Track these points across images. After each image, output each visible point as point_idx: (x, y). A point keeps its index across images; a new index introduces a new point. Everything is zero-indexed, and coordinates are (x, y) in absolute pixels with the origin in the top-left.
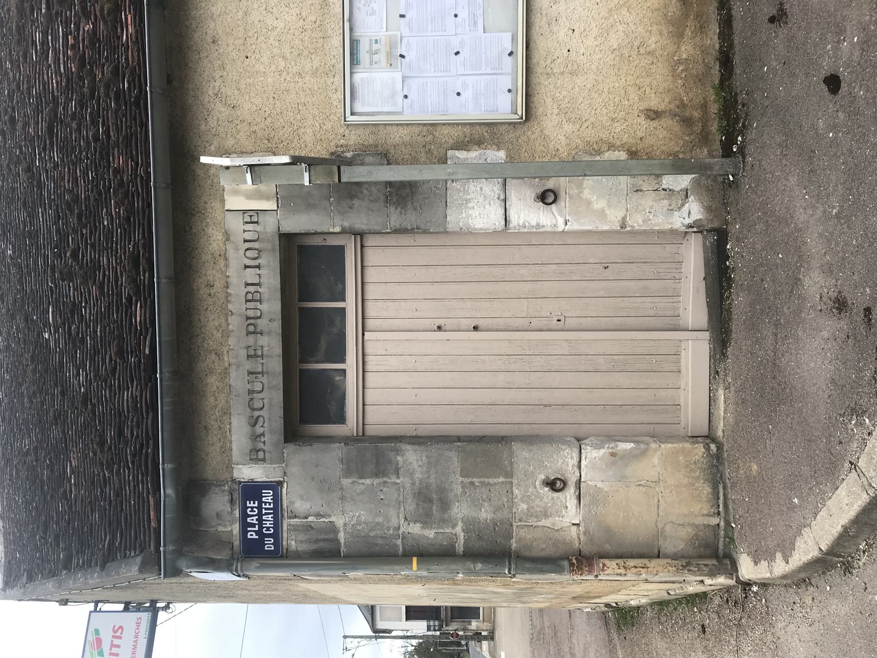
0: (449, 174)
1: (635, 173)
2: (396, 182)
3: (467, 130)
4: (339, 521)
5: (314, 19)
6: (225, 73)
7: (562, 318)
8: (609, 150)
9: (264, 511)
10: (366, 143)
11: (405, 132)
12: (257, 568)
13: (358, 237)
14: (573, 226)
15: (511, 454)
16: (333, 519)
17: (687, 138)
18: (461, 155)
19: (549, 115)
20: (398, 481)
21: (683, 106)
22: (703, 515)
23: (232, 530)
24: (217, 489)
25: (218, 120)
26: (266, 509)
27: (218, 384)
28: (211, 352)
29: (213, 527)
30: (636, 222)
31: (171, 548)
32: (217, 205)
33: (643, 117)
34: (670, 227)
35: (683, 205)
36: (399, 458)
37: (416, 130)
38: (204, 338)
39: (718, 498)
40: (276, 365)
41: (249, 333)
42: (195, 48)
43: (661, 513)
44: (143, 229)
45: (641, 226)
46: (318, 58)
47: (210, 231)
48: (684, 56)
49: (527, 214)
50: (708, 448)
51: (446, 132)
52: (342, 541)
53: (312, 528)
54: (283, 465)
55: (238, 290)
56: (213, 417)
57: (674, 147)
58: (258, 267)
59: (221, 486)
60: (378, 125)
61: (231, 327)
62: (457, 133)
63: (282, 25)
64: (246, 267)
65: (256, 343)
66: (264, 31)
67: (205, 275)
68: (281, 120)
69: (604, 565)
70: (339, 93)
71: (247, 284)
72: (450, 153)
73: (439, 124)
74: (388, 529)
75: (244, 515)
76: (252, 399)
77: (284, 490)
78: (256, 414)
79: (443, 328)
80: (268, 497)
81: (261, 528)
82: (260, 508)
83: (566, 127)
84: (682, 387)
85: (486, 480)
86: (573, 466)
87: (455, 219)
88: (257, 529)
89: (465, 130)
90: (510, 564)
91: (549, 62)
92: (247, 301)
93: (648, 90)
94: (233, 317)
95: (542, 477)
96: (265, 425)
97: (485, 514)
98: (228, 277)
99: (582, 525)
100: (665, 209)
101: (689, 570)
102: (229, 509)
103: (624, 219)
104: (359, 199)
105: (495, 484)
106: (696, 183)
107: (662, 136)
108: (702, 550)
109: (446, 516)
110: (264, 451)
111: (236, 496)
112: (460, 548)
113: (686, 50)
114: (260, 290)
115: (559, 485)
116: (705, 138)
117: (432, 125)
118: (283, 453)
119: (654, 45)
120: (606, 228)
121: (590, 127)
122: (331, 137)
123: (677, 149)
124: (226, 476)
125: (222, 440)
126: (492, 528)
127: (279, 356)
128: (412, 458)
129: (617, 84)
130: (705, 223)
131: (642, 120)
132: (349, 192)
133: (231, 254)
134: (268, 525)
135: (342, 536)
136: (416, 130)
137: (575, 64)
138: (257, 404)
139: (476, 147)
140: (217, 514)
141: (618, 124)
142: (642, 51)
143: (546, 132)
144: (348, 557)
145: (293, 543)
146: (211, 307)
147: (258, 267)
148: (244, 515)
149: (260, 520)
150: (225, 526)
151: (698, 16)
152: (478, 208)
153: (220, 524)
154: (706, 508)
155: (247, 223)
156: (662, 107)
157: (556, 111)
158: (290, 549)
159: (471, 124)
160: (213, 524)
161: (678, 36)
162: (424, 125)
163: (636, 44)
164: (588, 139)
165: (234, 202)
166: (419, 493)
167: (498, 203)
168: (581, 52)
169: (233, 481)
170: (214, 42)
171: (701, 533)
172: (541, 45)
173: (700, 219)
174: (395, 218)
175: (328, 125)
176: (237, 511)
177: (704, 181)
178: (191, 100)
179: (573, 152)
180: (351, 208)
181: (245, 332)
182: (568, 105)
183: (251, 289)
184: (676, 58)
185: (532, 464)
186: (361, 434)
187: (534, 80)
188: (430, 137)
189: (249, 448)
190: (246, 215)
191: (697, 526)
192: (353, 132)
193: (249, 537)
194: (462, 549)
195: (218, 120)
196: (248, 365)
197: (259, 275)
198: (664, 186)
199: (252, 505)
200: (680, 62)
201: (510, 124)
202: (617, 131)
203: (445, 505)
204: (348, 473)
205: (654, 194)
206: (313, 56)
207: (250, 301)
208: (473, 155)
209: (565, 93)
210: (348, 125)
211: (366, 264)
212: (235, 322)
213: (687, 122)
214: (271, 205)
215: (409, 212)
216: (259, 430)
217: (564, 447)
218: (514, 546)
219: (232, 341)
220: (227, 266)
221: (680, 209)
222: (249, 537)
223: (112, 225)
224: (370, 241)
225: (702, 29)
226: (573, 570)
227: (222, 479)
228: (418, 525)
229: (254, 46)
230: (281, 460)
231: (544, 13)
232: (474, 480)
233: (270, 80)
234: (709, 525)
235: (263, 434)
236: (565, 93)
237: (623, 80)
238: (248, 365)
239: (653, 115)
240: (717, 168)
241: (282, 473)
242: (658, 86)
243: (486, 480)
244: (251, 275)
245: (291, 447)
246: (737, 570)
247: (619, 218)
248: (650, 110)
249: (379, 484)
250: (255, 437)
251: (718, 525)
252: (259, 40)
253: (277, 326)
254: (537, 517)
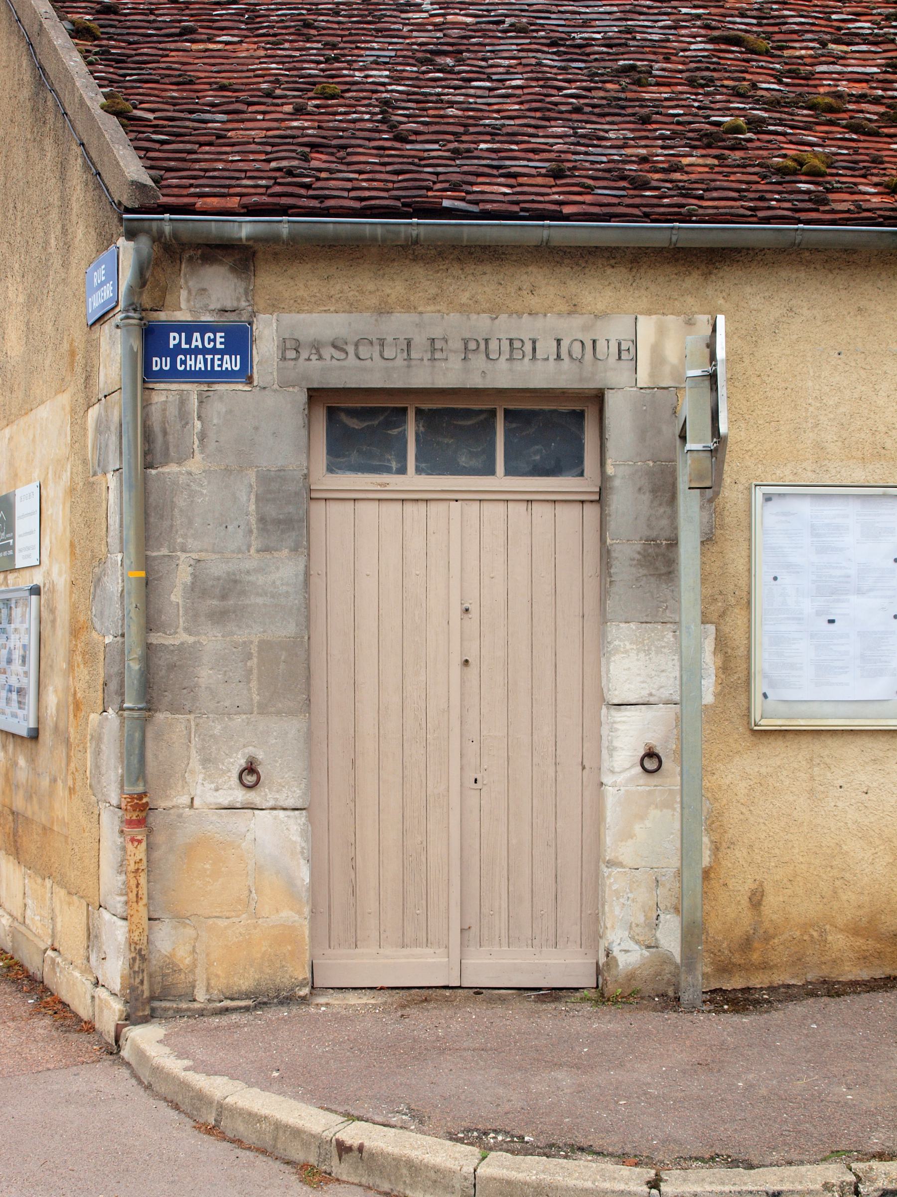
0: (688, 628)
1: (685, 874)
2: (677, 553)
3: (741, 651)
4: (196, 464)
5: (888, 446)
6: (819, 323)
7: (479, 786)
8: (712, 842)
9: (209, 357)
10: (726, 513)
11: (740, 567)
12: (132, 348)
13: (596, 497)
14: (610, 793)
15: (291, 713)
16: (198, 456)
17: (725, 945)
18: (709, 645)
19: (759, 761)
20: (252, 551)
21: (767, 938)
22: (208, 979)
23: (180, 309)
24: (242, 291)
25: (758, 311)
26: (213, 360)
27: (393, 296)
28: (440, 287)
29: (186, 282)
30: (614, 881)
31: (167, 228)
32: (644, 303)
33: (754, 886)
34: (609, 925)
35: (637, 942)
36: (286, 552)
37: (743, 583)
38: (459, 278)
39: (232, 999)
40: (420, 379)
41: (466, 342)
42: (852, 284)
43: (210, 921)
44: (614, 205)
45: (610, 887)
46: (838, 451)
47: (608, 293)
48: (830, 938)
49: (629, 734)
50: (302, 985)
51: (739, 622)
52: (166, 469)
53: (184, 426)
54: (276, 386)
55: (526, 328)
56: (346, 288)
57: (715, 925)
58: (559, 357)
59: (246, 294)
60: (750, 530)
61: (474, 317)
62: (738, 637)
63: (881, 403)
64: (559, 341)
65: (451, 351)
66: (873, 379)
67: (547, 284)
68: (757, 397)
69: (140, 842)
70: (791, 477)
71: (534, 342)
72: (711, 628)
73: (750, 613)
74: (184, 536)
75: (203, 328)
76: (371, 343)
77: (240, 387)
78: (351, 349)
79: (465, 616)
80: (230, 363)
81: (186, 352)
82: (214, 351)
83: (743, 784)
84: (381, 951)
85: (254, 676)
86: (276, 799)
87: (622, 634)
88: (184, 346)
89: (742, 649)
90: (140, 709)
91: (828, 761)
92: (511, 340)
93: (789, 892)
94: (488, 321)
95: (260, 755)
96: (334, 361)
97: (206, 676)
98: (545, 315)
99: (192, 812)
100: (632, 919)
101: (134, 959)
102: (212, 307)
103: (620, 865)
104: (652, 502)
105: (249, 689)
106: (667, 959)
107: (730, 914)
108: (159, 979)
109: (203, 618)
110: (296, 359)
111: (232, 317)
112: (156, 639)
113: (838, 941)
114: (526, 360)
115: (250, 779)
116: (724, 969)
117: (749, 603)
118: (294, 386)
119: (844, 898)
120: (609, 840)
121: (742, 817)
122: (733, 465)
123: (711, 932)
124: (261, 304)
125: (313, 300)
126: (185, 685)
127: (433, 384)
128: (285, 570)
129: (796, 851)
130: (614, 972)
131: (750, 885)
132: (663, 488)
133: (577, 321)
134: (189, 363)
135: (172, 469)
136: (743, 583)
137: (822, 796)
138: (364, 351)
139: (720, 664)
140: (204, 290)
141: (745, 854)
142: (838, 883)
143: (737, 759)
144: (145, 479)
145: (163, 399)
146: (501, 290)
147: (559, 357)
148: (203, 328)
149: (196, 351)
150: (188, 301)
151: (880, 955)
152: (640, 669)
153: (190, 292)
154: (220, 984)
155: (619, 344)
156: (766, 910)
157: (764, 770)
158: (154, 393)
159: (749, 657)
160: (191, 284)
161: (855, 930)
162: (749, 593)
163: (848, 876)
164: (727, 815)
165: (647, 327)
166: (235, 581)
167: (645, 693)
168: (839, 804)
169: (254, 314)
170: (859, 309)
171: (183, 976)
172: (851, 750)
173: (617, 965)
174: (625, 551)
175: (750, 462)
176: (209, 319)
177: (668, 968)
178: (784, 274)
179: (709, 795)
180: (640, 489)
181: (467, 336)
182: (771, 788)
183: (528, 347)
184: (828, 927)
185: (276, 742)
186: (314, 495)
187: (805, 741)
188: (733, 601)
189: (301, 339)
190: (630, 344)
191: (192, 971)
192: (740, 496)
193: (172, 335)
194: (155, 642)
195: (758, 311)
196: (420, 340)
197: (547, 359)
198: (662, 917)
199: (219, 340)
200: (823, 932)
201: (749, 709)
202: (736, 852)
203: (220, 617)
204: (265, 479)
205: (652, 903)
206: (839, 444)
207: (511, 344)
208: (709, 661)
209: (787, 783)
210: (749, 489)
211: (559, 506)
212: (481, 324)
213: (747, 944)
214: (643, 377)
215: (634, 570)
216: (328, 352)
217: (303, 786)
218: (160, 717)
219: (454, 317)
220: (560, 314)
221: (632, 938)
222: (172, 335)
223: (611, 147)
224: (591, 512)
225: (864, 959)
226: (132, 798)
227: (256, 298)
228: (189, 579)
229: (853, 364)
230: (284, 384)
231: (890, 754)
232: (255, 660)
233: (810, 384)
234: (194, 987)
235: (320, 358)
236: (787, 783)
237: (801, 859)
238: (420, 340)
239: (756, 900)
240: (689, 979)
241: (261, 384)
242: (791, 907)
243: (254, 676)
244: (547, 347)
245: (303, 397)
246: (135, 1023)
247: (621, 858)
248: (762, 896)
249: (248, 523)
250: (316, 347)
251: (195, 1000)
252: (862, 372)
253: (476, 381)
254: (204, 748)
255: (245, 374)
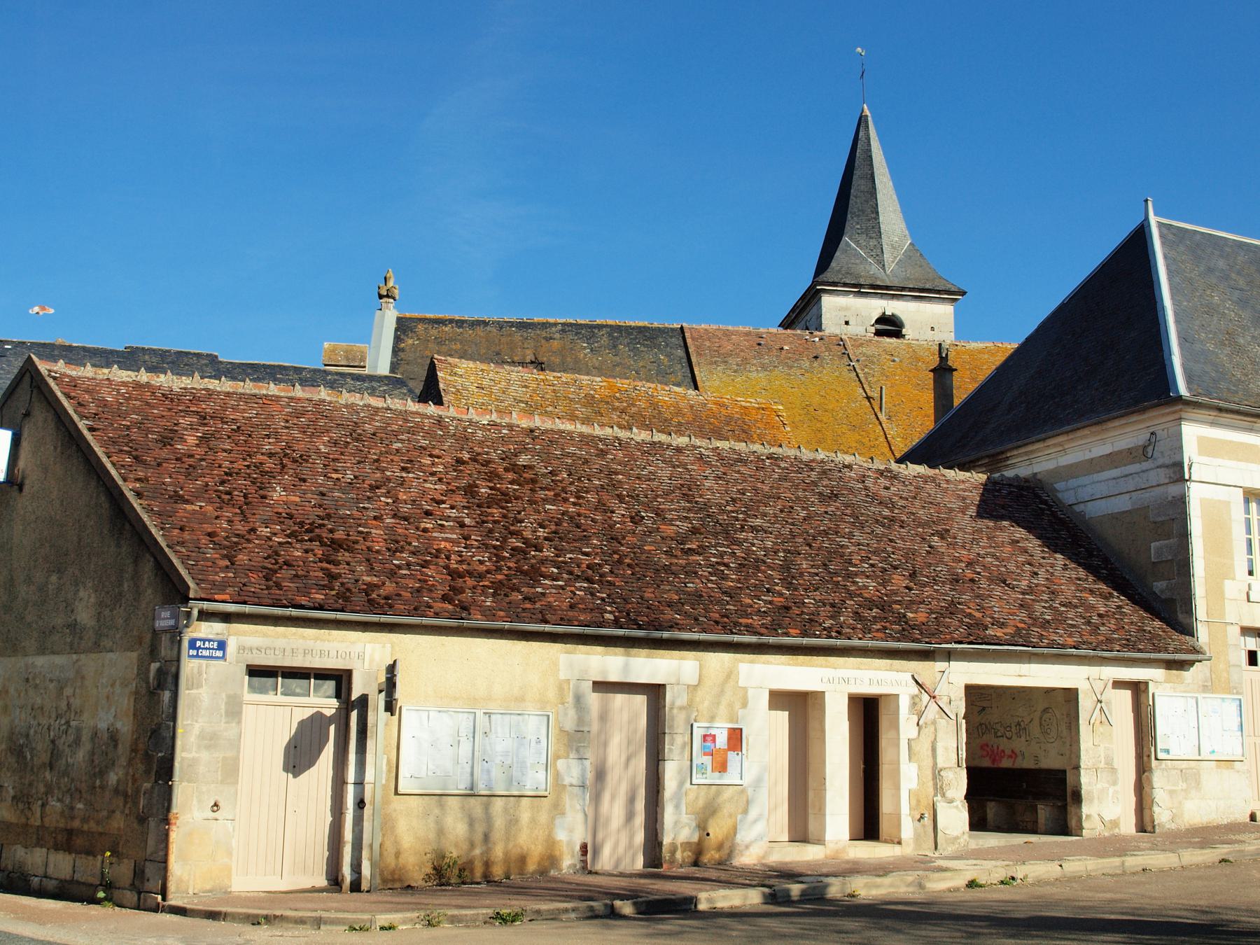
75: (210, 641)
80: (219, 654)
97: (202, 769)
165: (369, 647)
203: (208, 747)
212: (310, 644)
230: (238, 662)
255: (223, 658)
